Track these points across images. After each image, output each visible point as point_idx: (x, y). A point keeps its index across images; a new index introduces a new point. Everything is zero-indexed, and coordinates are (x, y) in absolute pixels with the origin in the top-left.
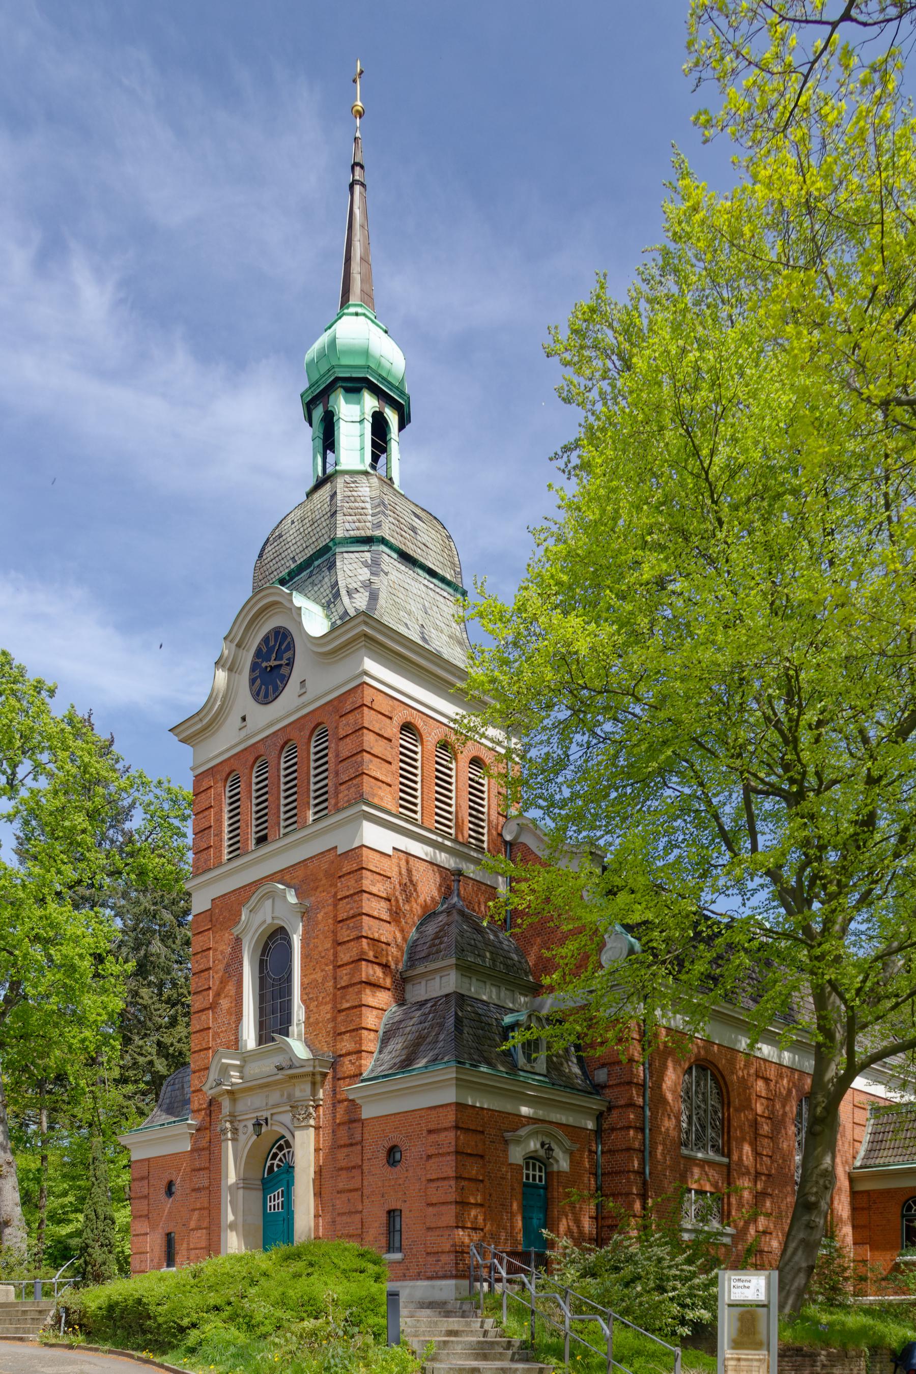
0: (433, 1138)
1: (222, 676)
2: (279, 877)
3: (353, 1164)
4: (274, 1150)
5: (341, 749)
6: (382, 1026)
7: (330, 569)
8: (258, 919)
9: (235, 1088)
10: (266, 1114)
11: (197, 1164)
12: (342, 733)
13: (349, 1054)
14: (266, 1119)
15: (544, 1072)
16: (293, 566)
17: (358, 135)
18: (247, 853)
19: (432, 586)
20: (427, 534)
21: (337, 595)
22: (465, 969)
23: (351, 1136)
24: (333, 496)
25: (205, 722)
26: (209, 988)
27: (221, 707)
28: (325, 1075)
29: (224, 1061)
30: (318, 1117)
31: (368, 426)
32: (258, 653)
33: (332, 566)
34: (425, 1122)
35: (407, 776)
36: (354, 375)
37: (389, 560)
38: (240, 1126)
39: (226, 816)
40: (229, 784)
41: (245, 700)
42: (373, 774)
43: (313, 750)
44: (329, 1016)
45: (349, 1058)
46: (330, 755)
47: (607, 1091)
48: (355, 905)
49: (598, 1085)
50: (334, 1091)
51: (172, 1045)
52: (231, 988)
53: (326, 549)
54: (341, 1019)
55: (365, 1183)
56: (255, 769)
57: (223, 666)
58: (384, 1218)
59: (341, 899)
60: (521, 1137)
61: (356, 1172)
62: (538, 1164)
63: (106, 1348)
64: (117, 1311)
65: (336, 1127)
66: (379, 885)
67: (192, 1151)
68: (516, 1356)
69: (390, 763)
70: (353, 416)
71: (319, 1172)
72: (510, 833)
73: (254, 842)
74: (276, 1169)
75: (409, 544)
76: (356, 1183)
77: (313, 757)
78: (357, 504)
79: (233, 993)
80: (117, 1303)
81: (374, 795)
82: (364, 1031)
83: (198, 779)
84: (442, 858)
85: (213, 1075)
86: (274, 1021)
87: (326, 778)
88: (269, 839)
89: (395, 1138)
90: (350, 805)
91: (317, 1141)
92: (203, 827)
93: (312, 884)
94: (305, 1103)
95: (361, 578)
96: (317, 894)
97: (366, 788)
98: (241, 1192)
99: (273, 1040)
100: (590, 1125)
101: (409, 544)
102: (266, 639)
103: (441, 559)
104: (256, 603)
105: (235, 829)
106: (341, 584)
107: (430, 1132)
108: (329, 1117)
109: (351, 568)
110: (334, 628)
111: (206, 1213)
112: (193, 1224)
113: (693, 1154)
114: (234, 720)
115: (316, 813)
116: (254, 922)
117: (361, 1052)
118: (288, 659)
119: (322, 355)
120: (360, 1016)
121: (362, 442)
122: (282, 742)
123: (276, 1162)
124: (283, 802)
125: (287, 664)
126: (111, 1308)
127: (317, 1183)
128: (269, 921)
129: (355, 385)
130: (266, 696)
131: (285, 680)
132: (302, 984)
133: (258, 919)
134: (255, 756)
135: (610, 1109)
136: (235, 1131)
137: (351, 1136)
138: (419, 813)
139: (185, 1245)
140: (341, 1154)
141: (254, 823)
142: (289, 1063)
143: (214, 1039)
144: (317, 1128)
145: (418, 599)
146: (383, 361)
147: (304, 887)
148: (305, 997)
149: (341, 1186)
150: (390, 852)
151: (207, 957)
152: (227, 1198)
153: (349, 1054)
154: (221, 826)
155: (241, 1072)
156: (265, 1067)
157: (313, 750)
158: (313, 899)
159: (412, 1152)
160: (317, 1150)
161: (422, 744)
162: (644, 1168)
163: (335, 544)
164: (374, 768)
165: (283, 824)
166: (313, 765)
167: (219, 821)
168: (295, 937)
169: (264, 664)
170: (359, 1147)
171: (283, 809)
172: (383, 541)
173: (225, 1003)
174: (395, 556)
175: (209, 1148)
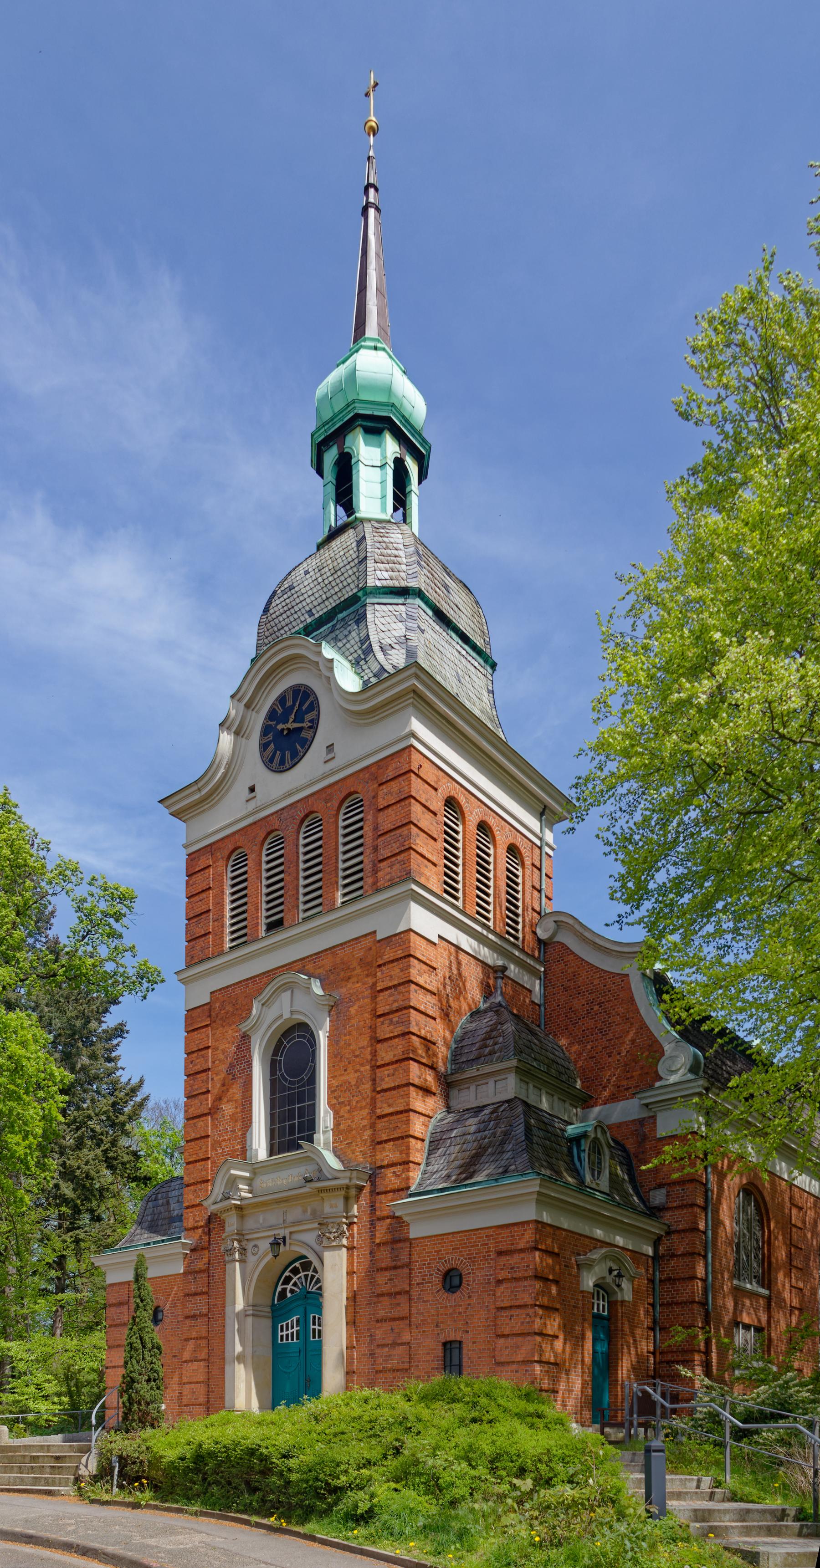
0: (503, 1260)
1: (227, 740)
2: (299, 965)
3: (397, 1289)
4: (287, 1274)
5: (380, 820)
6: (428, 1135)
7: (358, 622)
8: (271, 1014)
9: (244, 1202)
10: (282, 1233)
11: (192, 1289)
12: (382, 803)
13: (392, 1165)
14: (284, 1238)
15: (607, 1190)
16: (309, 620)
17: (371, 154)
18: (256, 940)
19: (464, 653)
20: (458, 596)
21: (369, 650)
22: (524, 1073)
23: (395, 1258)
24: (362, 540)
25: (204, 792)
26: (208, 1092)
27: (225, 775)
28: (360, 1189)
29: (233, 1172)
30: (352, 1235)
31: (390, 472)
32: (272, 715)
33: (361, 618)
34: (501, 1244)
35: (450, 857)
36: (376, 413)
37: (426, 618)
38: (249, 1246)
39: (228, 899)
40: (231, 863)
41: (253, 766)
42: (420, 850)
43: (341, 824)
44: (365, 1122)
45: (392, 1169)
46: (366, 828)
47: (668, 1214)
48: (400, 997)
49: (655, 1208)
50: (373, 1207)
51: (79, 1168)
52: (236, 1091)
53: (354, 600)
54: (385, 1127)
55: (414, 1311)
56: (266, 846)
57: (228, 728)
58: (439, 1351)
59: (381, 991)
60: (594, 1261)
61: (402, 1299)
62: (601, 1292)
63: (195, 1508)
64: (211, 1464)
65: (375, 1248)
66: (425, 976)
67: (185, 1273)
68: (805, 1530)
69: (435, 840)
70: (373, 460)
71: (353, 1298)
72: (545, 931)
73: (264, 928)
74: (289, 1295)
75: (443, 602)
76: (403, 1310)
77: (341, 832)
78: (389, 551)
79: (238, 1096)
80: (212, 1454)
81: (421, 874)
82: (411, 1140)
83: (192, 858)
84: (485, 953)
85: (218, 1189)
86: (292, 1127)
87: (361, 854)
88: (286, 923)
89: (453, 1259)
90: (392, 884)
91: (350, 1263)
92: (198, 911)
93: (342, 974)
94: (338, 1220)
95: (396, 634)
96: (350, 985)
97: (413, 866)
98: (250, 1320)
99: (299, 1147)
100: (650, 1251)
101: (443, 602)
102: (282, 699)
103: (472, 625)
104: (274, 655)
105: (239, 913)
106: (373, 638)
107: (500, 1253)
108: (367, 1236)
109: (384, 622)
110: (367, 687)
111: (203, 1343)
112: (186, 1355)
113: (742, 1284)
114: (239, 790)
115: (345, 895)
116: (267, 1018)
117: (407, 1162)
118: (311, 721)
119: (339, 389)
120: (408, 1122)
121: (384, 489)
122: (302, 815)
123: (289, 1287)
124: (302, 882)
125: (310, 727)
126: (200, 1457)
127: (351, 1310)
128: (287, 1015)
129: (378, 424)
130: (282, 762)
131: (307, 744)
132: (329, 1087)
133: (271, 1014)
134: (268, 831)
135: (668, 1233)
136: (243, 1251)
137: (395, 1258)
138: (461, 900)
139: (176, 1379)
140: (381, 1279)
141: (264, 906)
142: (318, 1174)
143: (214, 1148)
144: (350, 1249)
145: (452, 665)
146: (405, 401)
147: (332, 977)
148: (334, 1101)
149: (382, 1314)
150: (435, 940)
151: (205, 1057)
152: (233, 1326)
153: (392, 1165)
154: (222, 910)
155: (249, 1185)
156: (289, 1176)
157: (341, 824)
158: (344, 990)
159: (476, 1276)
160: (350, 1273)
161: (464, 824)
162: (707, 1299)
163: (366, 594)
164: (421, 843)
165: (302, 907)
166: (341, 840)
167: (220, 904)
168: (321, 1033)
169: (280, 727)
170: (406, 1270)
171: (302, 891)
172: (419, 593)
173: (228, 1109)
174: (430, 613)
175: (207, 1270)
